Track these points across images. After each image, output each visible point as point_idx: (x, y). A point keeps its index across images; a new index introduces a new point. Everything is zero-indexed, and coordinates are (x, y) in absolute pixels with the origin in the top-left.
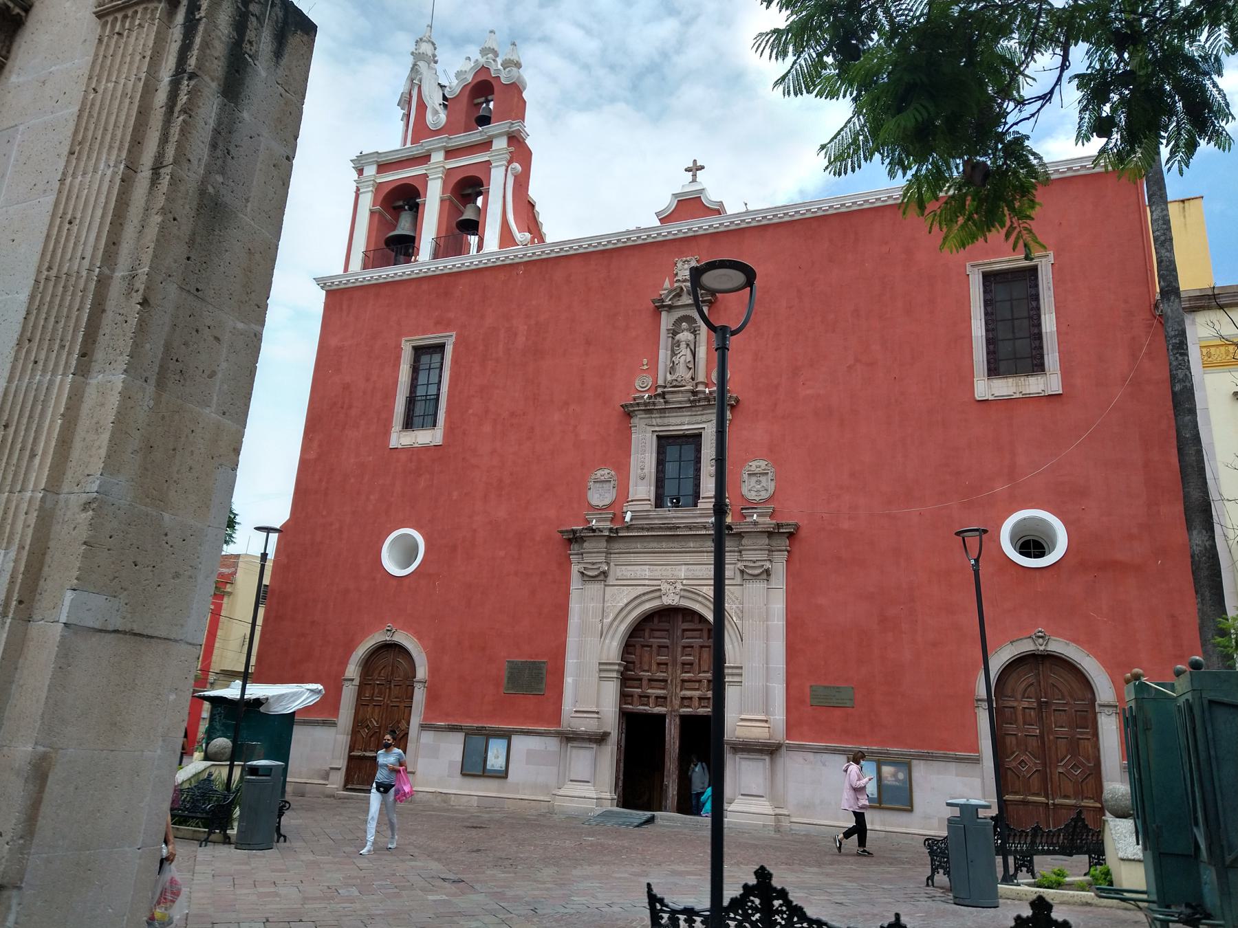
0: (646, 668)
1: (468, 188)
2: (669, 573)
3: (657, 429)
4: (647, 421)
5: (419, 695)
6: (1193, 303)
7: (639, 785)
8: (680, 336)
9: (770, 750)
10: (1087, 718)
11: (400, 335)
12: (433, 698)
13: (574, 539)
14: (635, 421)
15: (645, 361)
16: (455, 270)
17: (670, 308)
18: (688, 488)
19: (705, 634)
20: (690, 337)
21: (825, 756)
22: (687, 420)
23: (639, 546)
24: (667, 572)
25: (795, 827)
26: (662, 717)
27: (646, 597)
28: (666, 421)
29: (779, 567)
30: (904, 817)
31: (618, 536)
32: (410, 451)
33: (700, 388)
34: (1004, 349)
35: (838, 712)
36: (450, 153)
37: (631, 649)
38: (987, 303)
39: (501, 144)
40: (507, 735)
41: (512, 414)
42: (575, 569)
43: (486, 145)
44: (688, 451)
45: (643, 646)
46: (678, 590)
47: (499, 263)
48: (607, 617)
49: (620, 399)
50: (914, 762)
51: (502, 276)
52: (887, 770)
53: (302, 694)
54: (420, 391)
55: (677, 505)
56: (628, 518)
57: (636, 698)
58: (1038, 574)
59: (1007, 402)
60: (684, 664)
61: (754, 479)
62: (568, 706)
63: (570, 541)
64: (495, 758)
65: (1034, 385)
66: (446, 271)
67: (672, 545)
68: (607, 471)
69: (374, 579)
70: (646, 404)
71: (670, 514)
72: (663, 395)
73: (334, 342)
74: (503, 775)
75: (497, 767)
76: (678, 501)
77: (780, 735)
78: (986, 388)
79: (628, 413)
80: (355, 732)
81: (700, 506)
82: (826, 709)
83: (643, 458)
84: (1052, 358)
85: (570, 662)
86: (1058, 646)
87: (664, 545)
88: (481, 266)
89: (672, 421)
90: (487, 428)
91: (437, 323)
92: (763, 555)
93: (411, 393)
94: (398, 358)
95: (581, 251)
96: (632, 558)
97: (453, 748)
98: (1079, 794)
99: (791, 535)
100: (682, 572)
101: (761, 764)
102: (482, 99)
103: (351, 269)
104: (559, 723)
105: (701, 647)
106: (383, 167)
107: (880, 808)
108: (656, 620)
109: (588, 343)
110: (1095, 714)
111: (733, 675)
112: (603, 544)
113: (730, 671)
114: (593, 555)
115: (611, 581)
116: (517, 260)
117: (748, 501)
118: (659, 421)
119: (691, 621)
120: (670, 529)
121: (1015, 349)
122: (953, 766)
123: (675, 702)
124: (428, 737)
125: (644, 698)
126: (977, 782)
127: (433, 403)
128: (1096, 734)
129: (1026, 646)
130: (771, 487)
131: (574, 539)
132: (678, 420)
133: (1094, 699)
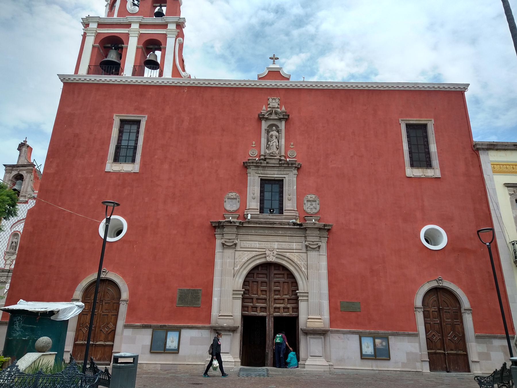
0: (255, 293)
1: (152, 45)
2: (269, 246)
3: (261, 175)
4: (256, 171)
5: (123, 309)
6: (488, 147)
7: (253, 353)
8: (271, 133)
9: (322, 333)
10: (458, 315)
11: (112, 112)
12: (132, 309)
13: (218, 226)
14: (249, 170)
15: (254, 143)
16: (147, 84)
17: (267, 119)
18: (276, 205)
19: (286, 276)
20: (277, 134)
21: (349, 336)
22: (276, 172)
23: (253, 231)
24: (268, 245)
25: (336, 371)
26: (264, 318)
27: (258, 257)
28: (266, 172)
29: (323, 245)
30: (386, 363)
31: (243, 225)
32: (118, 174)
33: (283, 158)
34: (415, 156)
35: (353, 314)
36: (142, 26)
37: (246, 283)
38: (408, 137)
39: (172, 27)
40: (178, 329)
41: (181, 161)
42: (218, 242)
43: (165, 26)
44: (134, 128)
45: (253, 282)
46: (275, 254)
47: (173, 84)
48: (237, 266)
49: (241, 160)
50: (390, 337)
51: (175, 91)
52: (378, 341)
53: (71, 309)
54: (124, 143)
55: (271, 213)
56: (249, 217)
57: (250, 309)
58: (436, 252)
59: (419, 178)
60: (275, 291)
61: (309, 203)
62: (215, 312)
63: (215, 227)
64: (172, 341)
65: (429, 173)
66: (142, 83)
67: (270, 232)
68: (234, 194)
69: (93, 243)
70: (257, 163)
71: (267, 216)
72: (265, 159)
73: (68, 110)
74: (176, 351)
75: (172, 347)
76: (273, 211)
77: (327, 327)
78: (410, 172)
79: (246, 166)
80: (429, 341)
81: (284, 214)
82: (347, 313)
83: (254, 188)
84: (435, 162)
85: (216, 289)
86: (447, 284)
87: (266, 232)
88: (163, 84)
89: (268, 172)
90: (166, 166)
91: (135, 109)
92: (317, 239)
93: (118, 143)
94: (111, 125)
95: (219, 86)
96: (250, 237)
97: (145, 338)
98: (456, 349)
99: (329, 230)
100: (276, 245)
101: (320, 340)
102: (159, 5)
103: (80, 72)
104: (209, 322)
105: (284, 282)
106: (101, 25)
107: (376, 359)
108: (260, 269)
109: (223, 130)
110: (461, 313)
111: (303, 296)
112: (235, 230)
113: (302, 294)
114: (229, 234)
115: (238, 248)
116: (184, 85)
117: (307, 213)
118: (262, 171)
119: (278, 270)
120: (271, 224)
121: (421, 158)
122: (406, 338)
123: (272, 309)
124: (128, 332)
125: (255, 308)
126: (417, 345)
127: (132, 151)
128: (462, 322)
129: (434, 284)
130: (318, 207)
131: (218, 226)
132: (272, 172)
133: (460, 308)
